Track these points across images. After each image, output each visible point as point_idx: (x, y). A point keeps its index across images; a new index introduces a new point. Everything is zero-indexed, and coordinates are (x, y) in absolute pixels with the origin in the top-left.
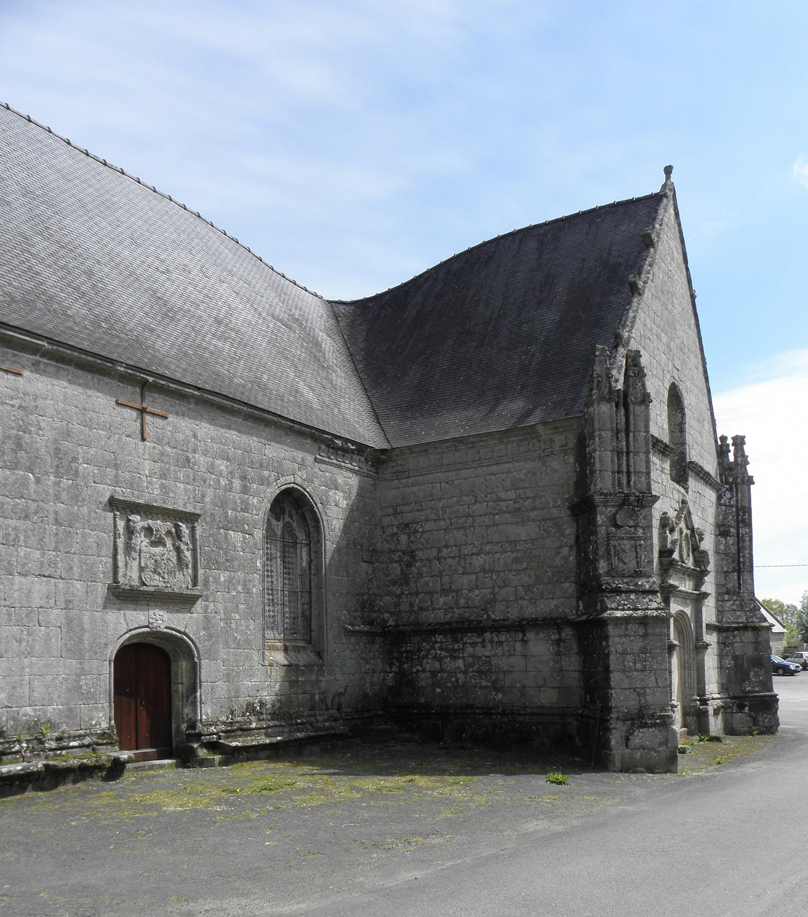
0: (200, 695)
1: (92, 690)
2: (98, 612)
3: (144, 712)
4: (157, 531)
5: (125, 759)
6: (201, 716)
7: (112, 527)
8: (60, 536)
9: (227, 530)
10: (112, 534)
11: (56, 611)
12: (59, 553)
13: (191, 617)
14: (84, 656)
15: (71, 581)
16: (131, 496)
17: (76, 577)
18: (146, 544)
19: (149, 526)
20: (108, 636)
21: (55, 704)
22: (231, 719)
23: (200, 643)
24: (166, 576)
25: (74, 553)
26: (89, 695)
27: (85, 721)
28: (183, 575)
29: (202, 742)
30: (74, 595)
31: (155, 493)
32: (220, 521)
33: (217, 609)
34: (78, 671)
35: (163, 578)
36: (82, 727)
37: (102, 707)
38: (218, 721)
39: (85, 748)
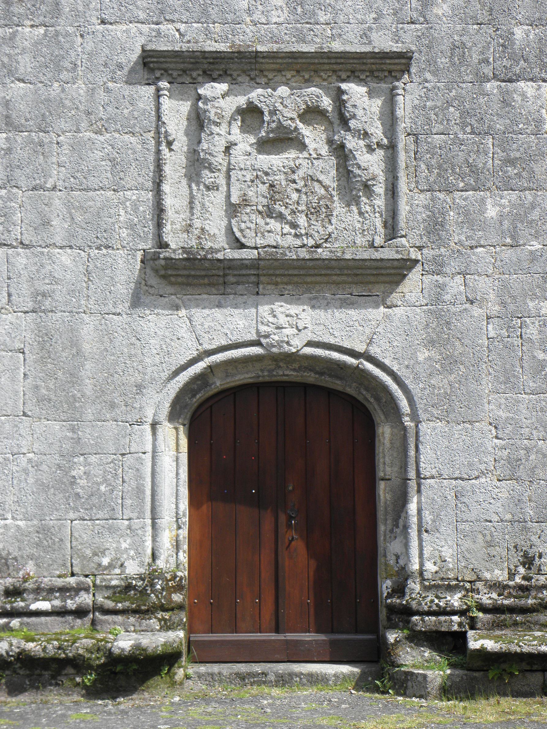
0: (419, 511)
1: (103, 488)
2: (119, 314)
3: (299, 546)
4: (273, 112)
5: (123, 650)
6: (422, 564)
7: (150, 121)
8: (20, 154)
9: (510, 81)
10: (152, 134)
11: (10, 317)
12: (15, 190)
13: (387, 317)
14: (82, 413)
15: (46, 250)
16: (201, 38)
17: (58, 240)
18: (249, 149)
19: (250, 103)
20: (145, 368)
21: (9, 516)
22: (524, 578)
23: (417, 378)
24: (302, 221)
25: (54, 188)
26: (95, 500)
27: (83, 557)
28: (361, 213)
29: (412, 630)
30: (55, 281)
31: (274, 20)
32: (486, 61)
33: (474, 290)
34: (67, 446)
35: (294, 226)
36: (76, 570)
37: (129, 527)
38: (479, 579)
39: (70, 618)
